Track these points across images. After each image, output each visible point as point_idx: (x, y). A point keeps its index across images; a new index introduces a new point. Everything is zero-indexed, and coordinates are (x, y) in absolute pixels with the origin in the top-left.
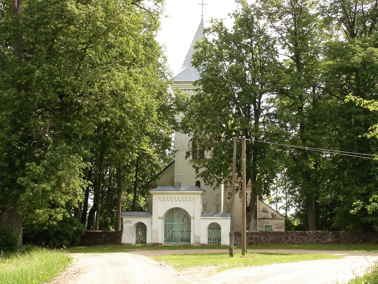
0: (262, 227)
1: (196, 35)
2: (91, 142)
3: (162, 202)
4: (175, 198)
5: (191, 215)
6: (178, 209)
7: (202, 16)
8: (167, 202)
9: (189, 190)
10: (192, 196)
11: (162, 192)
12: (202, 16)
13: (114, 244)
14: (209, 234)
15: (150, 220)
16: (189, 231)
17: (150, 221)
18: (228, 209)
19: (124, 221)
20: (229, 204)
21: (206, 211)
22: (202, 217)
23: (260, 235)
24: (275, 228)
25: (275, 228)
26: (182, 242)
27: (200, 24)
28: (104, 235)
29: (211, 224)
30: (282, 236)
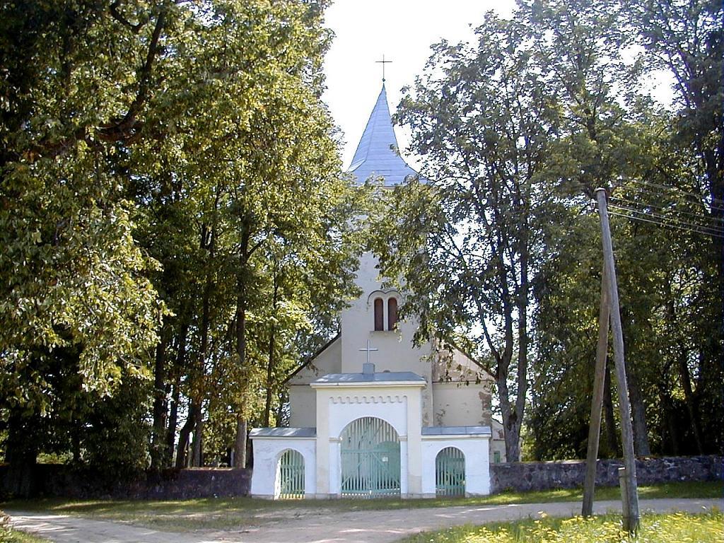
3: (337, 408)
5: (401, 434)
6: (369, 421)
10: (402, 393)
12: (384, 80)
17: (312, 446)
21: (436, 422)
26: (380, 491)
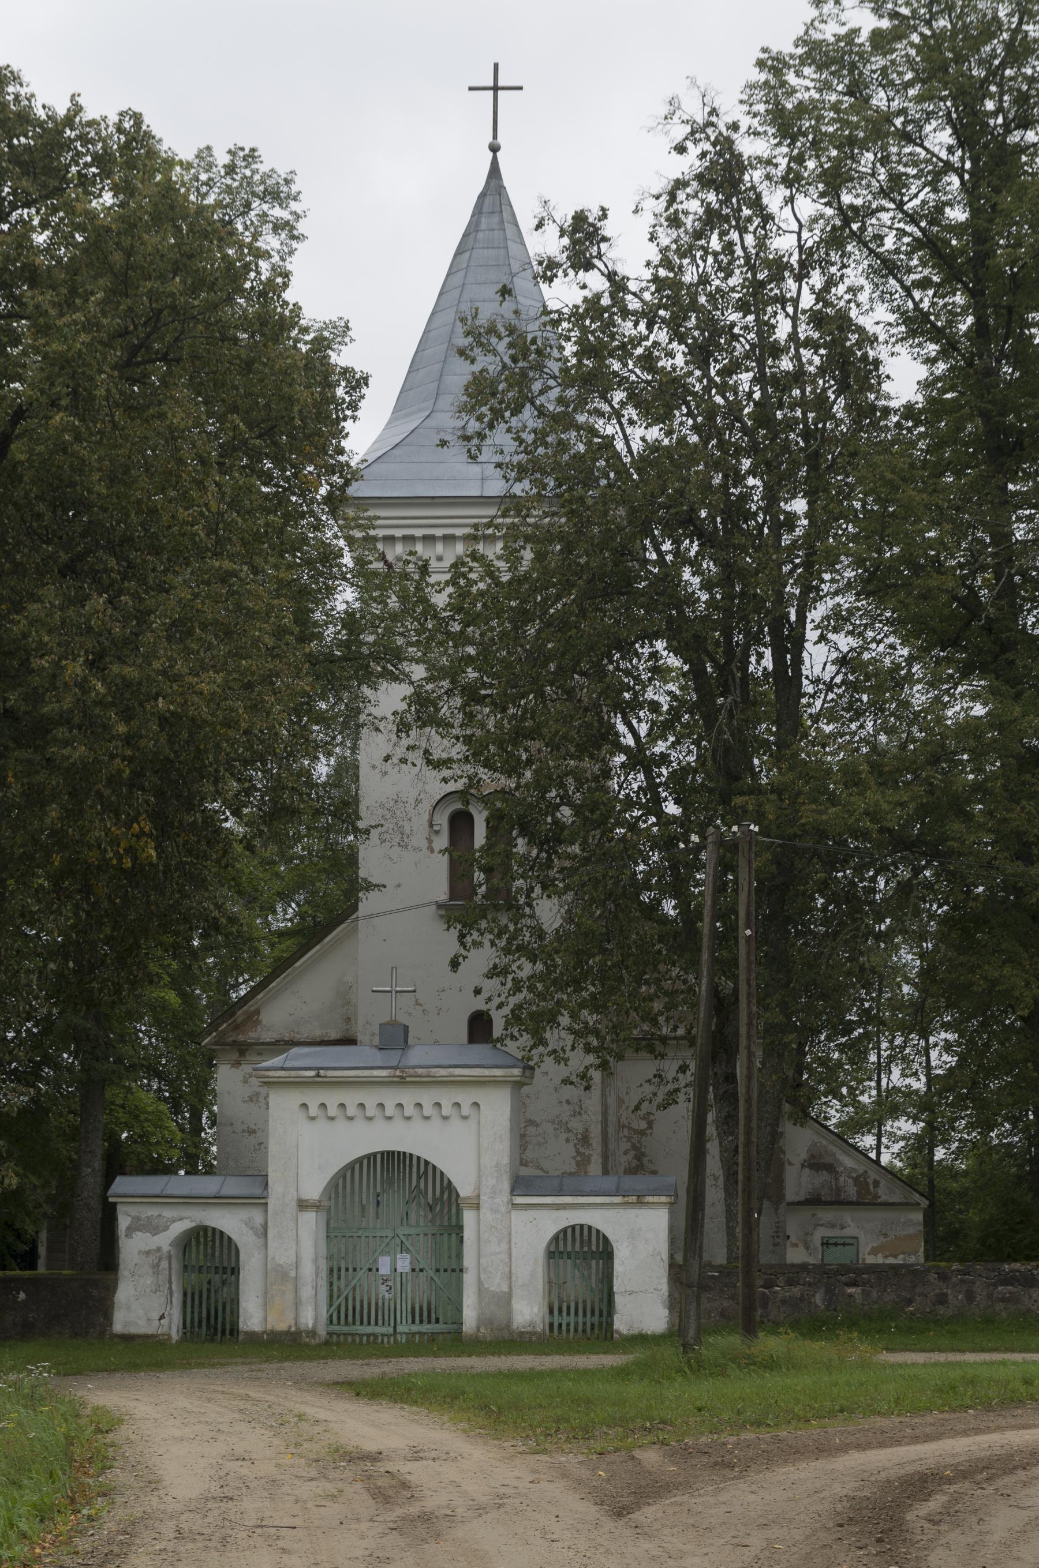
0: (807, 1248)
1: (458, 253)
2: (48, 808)
4: (400, 1106)
5: (465, 1190)
7: (494, 149)
8: (341, 1124)
9: (491, 1062)
11: (312, 1073)
12: (494, 149)
13: (75, 1335)
14: (552, 1284)
15: (257, 1216)
16: (453, 1270)
18: (632, 1153)
19: (123, 1222)
20: (637, 1132)
22: (519, 1200)
23: (810, 1284)
24: (874, 1252)
25: (874, 1252)
27: (482, 196)
28: (22, 1296)
29: (564, 1231)
30: (918, 1290)
